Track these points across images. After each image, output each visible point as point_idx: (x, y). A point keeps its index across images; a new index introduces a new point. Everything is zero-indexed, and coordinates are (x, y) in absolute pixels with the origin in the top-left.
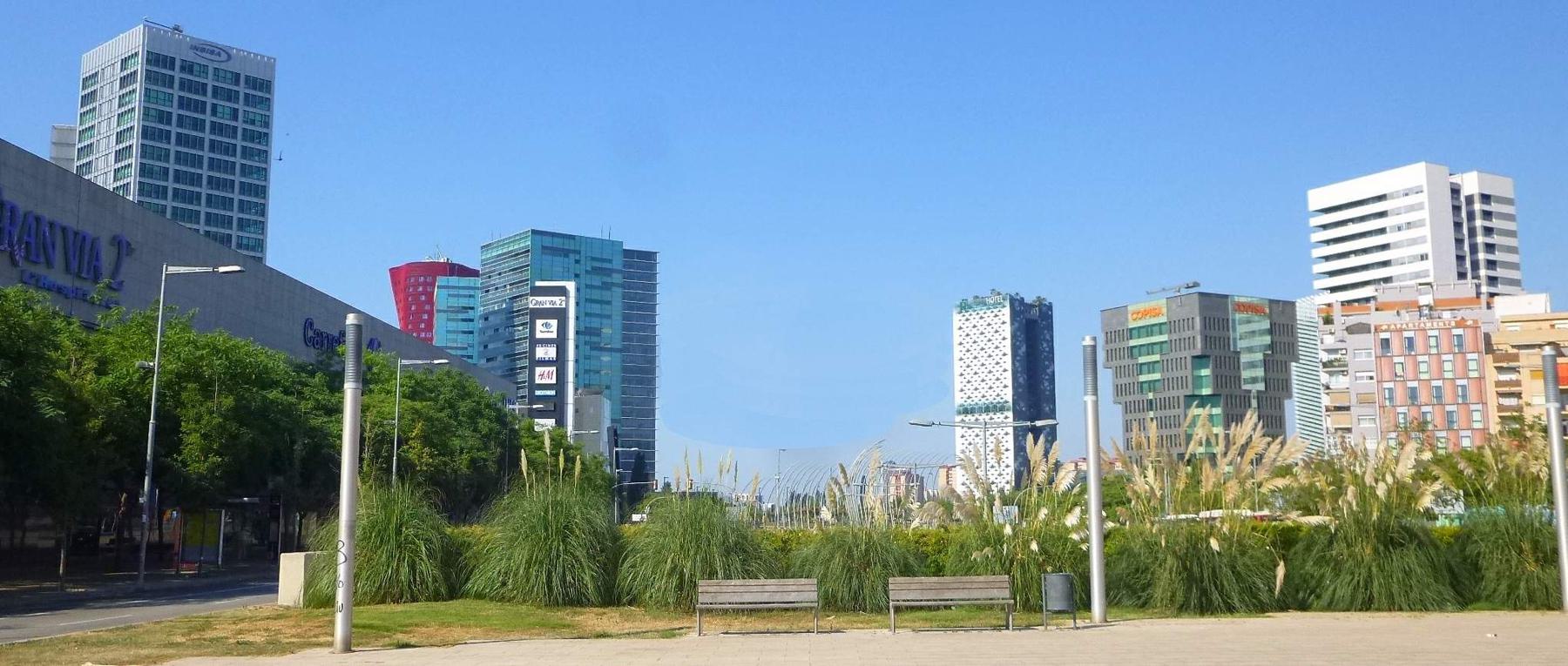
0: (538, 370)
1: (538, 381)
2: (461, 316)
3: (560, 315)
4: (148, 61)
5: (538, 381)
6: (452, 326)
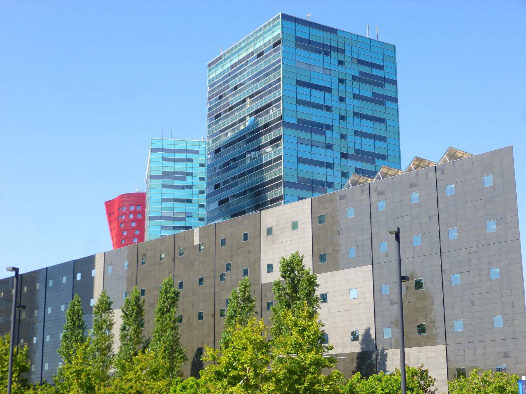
2: (177, 183)
6: (169, 193)
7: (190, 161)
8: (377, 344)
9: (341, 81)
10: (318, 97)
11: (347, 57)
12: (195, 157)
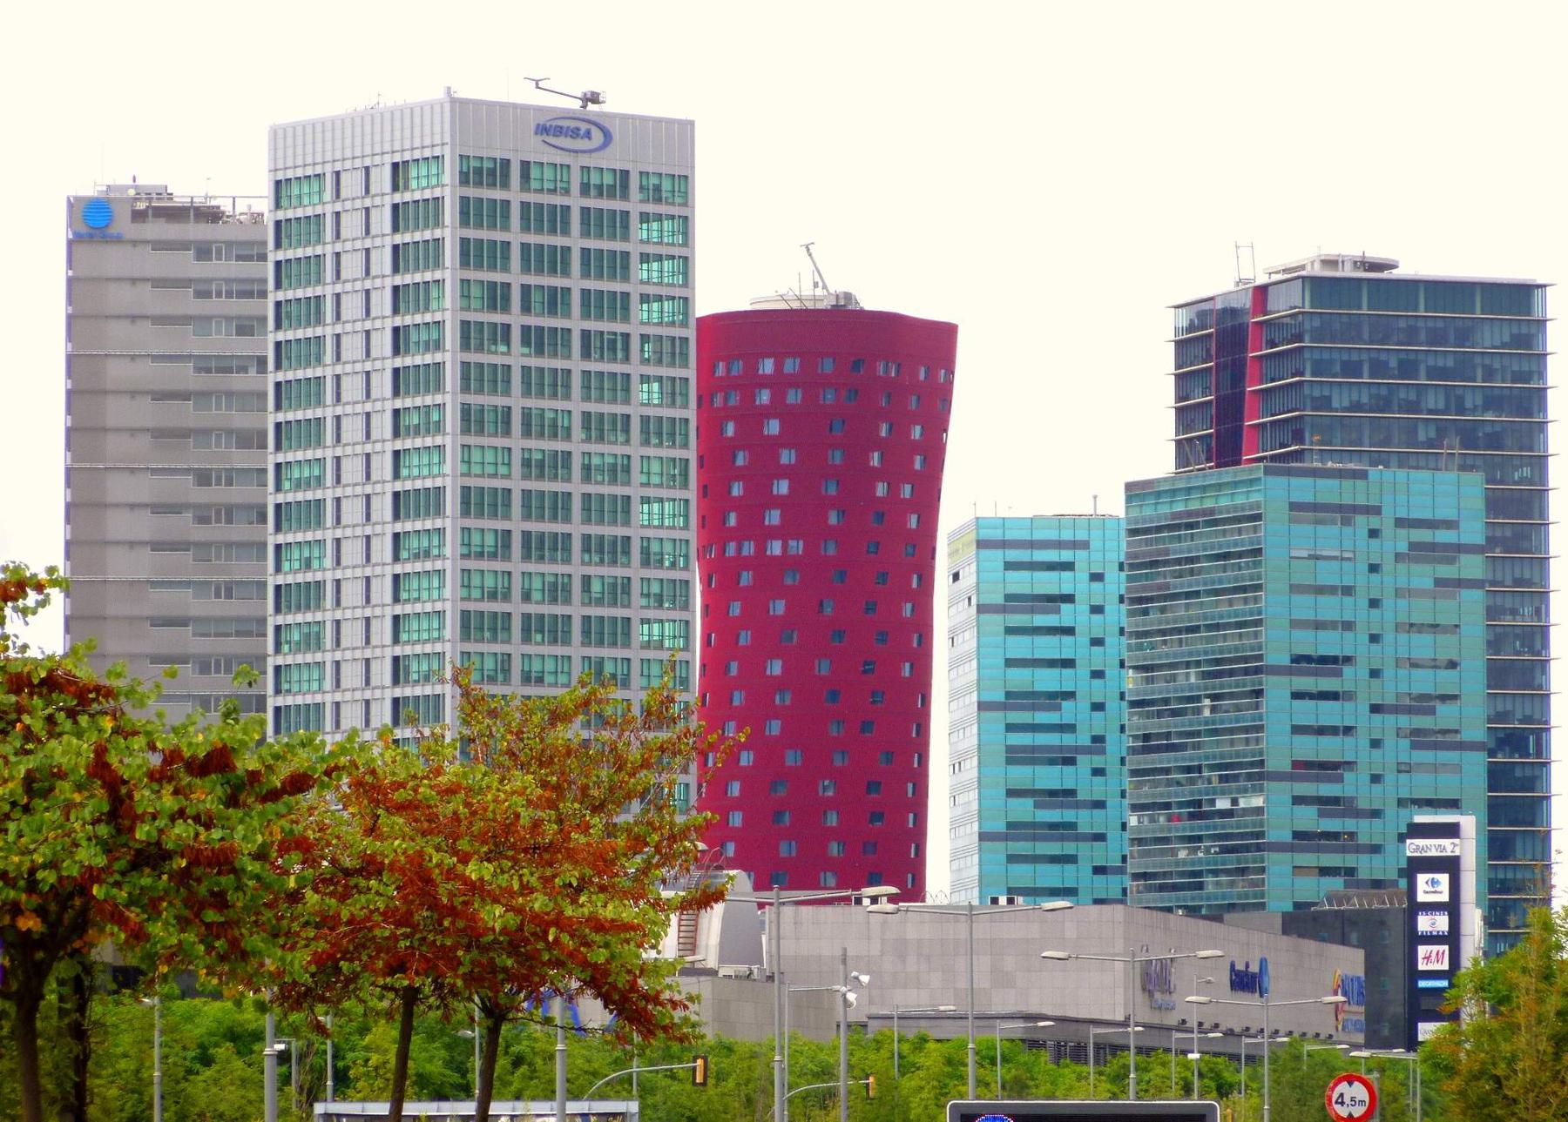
0: (1422, 950)
1: (1422, 966)
2: (1041, 620)
3: (1450, 865)
4: (464, 179)
5: (1422, 966)
7: (1068, 566)
8: (1059, 1013)
9: (1374, 568)
10: (1329, 608)
11: (1386, 522)
12: (1081, 555)
